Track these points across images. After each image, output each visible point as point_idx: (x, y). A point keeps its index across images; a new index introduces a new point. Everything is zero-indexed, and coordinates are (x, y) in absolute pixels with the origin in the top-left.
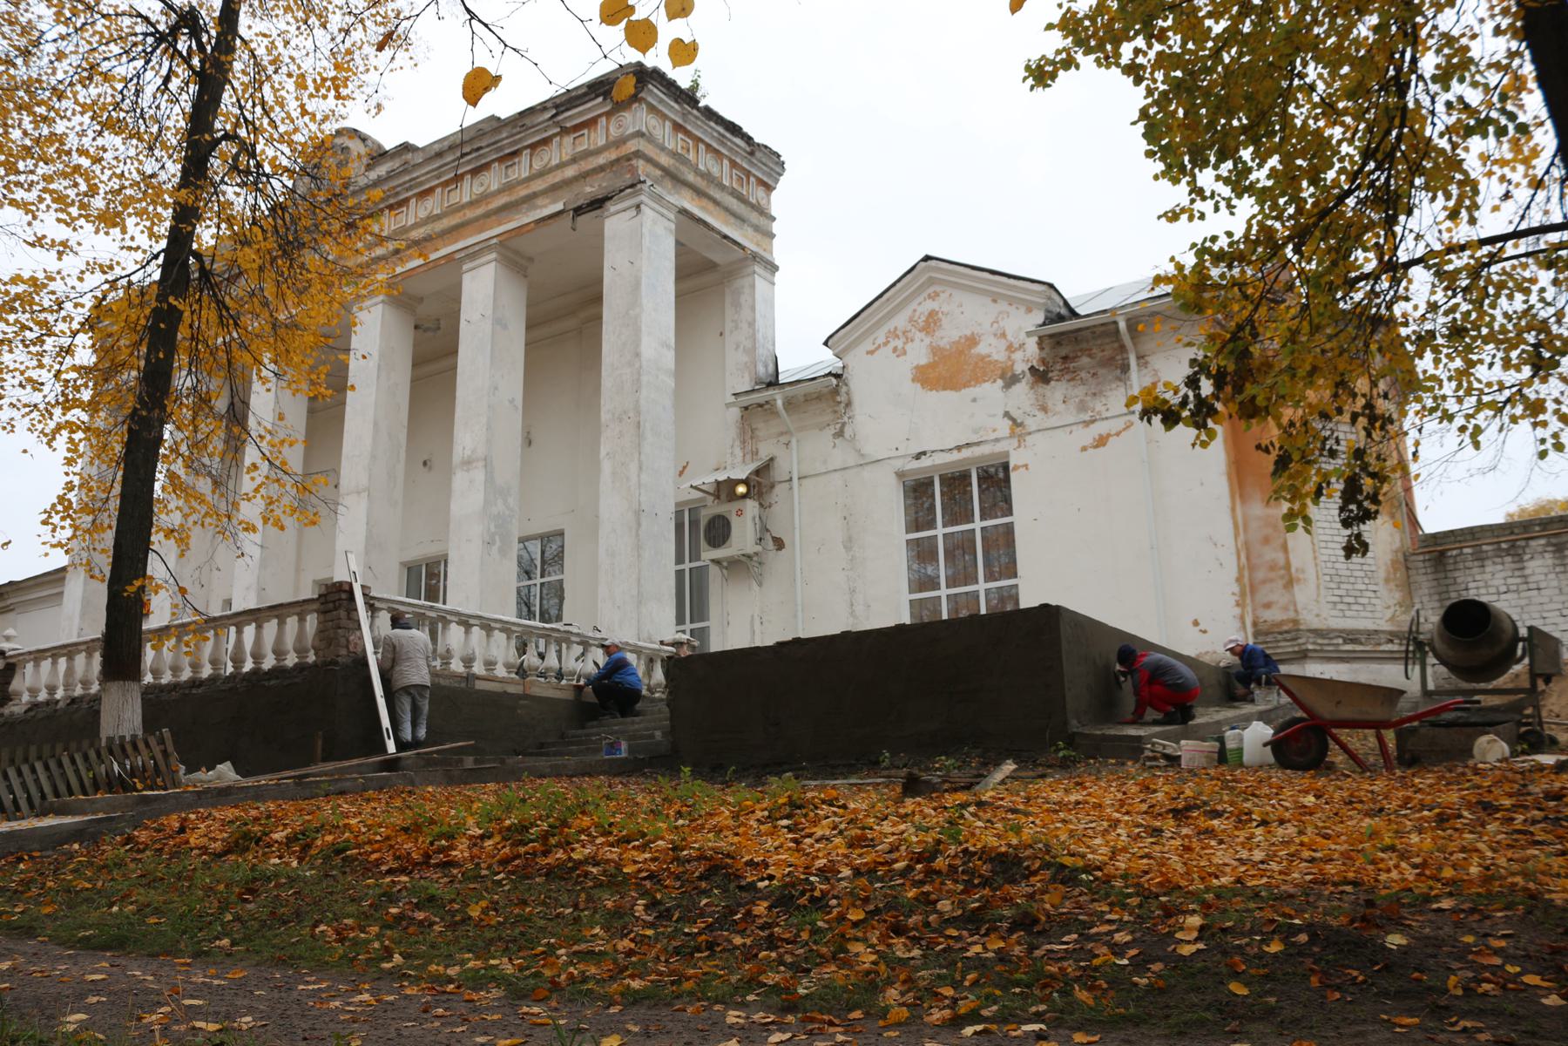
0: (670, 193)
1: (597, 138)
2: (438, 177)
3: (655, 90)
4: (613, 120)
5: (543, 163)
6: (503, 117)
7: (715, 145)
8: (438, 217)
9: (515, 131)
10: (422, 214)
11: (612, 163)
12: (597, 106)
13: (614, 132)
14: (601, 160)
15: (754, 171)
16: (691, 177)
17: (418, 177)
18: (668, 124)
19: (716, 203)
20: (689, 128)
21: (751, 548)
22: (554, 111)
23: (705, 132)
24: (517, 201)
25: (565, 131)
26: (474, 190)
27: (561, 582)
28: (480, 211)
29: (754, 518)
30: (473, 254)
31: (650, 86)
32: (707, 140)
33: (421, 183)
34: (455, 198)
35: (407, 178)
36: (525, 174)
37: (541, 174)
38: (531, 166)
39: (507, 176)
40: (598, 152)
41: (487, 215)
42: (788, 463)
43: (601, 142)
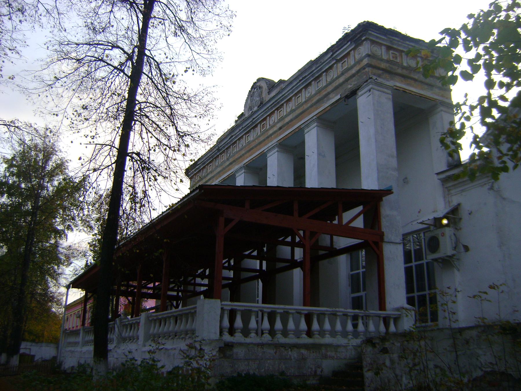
1: (351, 61)
2: (292, 92)
3: (373, 33)
4: (356, 52)
5: (331, 78)
6: (286, 79)
10: (289, 110)
11: (358, 71)
13: (357, 57)
14: (353, 71)
16: (399, 71)
17: (285, 94)
18: (383, 47)
19: (415, 80)
20: (395, 47)
21: (449, 251)
22: (331, 53)
25: (338, 61)
26: (306, 95)
27: (352, 270)
28: (309, 105)
29: (450, 237)
30: (307, 125)
31: (370, 32)
33: (286, 97)
35: (281, 95)
36: (324, 84)
37: (331, 83)
38: (326, 80)
40: (352, 67)
41: (311, 106)
42: (466, 207)
43: (352, 63)
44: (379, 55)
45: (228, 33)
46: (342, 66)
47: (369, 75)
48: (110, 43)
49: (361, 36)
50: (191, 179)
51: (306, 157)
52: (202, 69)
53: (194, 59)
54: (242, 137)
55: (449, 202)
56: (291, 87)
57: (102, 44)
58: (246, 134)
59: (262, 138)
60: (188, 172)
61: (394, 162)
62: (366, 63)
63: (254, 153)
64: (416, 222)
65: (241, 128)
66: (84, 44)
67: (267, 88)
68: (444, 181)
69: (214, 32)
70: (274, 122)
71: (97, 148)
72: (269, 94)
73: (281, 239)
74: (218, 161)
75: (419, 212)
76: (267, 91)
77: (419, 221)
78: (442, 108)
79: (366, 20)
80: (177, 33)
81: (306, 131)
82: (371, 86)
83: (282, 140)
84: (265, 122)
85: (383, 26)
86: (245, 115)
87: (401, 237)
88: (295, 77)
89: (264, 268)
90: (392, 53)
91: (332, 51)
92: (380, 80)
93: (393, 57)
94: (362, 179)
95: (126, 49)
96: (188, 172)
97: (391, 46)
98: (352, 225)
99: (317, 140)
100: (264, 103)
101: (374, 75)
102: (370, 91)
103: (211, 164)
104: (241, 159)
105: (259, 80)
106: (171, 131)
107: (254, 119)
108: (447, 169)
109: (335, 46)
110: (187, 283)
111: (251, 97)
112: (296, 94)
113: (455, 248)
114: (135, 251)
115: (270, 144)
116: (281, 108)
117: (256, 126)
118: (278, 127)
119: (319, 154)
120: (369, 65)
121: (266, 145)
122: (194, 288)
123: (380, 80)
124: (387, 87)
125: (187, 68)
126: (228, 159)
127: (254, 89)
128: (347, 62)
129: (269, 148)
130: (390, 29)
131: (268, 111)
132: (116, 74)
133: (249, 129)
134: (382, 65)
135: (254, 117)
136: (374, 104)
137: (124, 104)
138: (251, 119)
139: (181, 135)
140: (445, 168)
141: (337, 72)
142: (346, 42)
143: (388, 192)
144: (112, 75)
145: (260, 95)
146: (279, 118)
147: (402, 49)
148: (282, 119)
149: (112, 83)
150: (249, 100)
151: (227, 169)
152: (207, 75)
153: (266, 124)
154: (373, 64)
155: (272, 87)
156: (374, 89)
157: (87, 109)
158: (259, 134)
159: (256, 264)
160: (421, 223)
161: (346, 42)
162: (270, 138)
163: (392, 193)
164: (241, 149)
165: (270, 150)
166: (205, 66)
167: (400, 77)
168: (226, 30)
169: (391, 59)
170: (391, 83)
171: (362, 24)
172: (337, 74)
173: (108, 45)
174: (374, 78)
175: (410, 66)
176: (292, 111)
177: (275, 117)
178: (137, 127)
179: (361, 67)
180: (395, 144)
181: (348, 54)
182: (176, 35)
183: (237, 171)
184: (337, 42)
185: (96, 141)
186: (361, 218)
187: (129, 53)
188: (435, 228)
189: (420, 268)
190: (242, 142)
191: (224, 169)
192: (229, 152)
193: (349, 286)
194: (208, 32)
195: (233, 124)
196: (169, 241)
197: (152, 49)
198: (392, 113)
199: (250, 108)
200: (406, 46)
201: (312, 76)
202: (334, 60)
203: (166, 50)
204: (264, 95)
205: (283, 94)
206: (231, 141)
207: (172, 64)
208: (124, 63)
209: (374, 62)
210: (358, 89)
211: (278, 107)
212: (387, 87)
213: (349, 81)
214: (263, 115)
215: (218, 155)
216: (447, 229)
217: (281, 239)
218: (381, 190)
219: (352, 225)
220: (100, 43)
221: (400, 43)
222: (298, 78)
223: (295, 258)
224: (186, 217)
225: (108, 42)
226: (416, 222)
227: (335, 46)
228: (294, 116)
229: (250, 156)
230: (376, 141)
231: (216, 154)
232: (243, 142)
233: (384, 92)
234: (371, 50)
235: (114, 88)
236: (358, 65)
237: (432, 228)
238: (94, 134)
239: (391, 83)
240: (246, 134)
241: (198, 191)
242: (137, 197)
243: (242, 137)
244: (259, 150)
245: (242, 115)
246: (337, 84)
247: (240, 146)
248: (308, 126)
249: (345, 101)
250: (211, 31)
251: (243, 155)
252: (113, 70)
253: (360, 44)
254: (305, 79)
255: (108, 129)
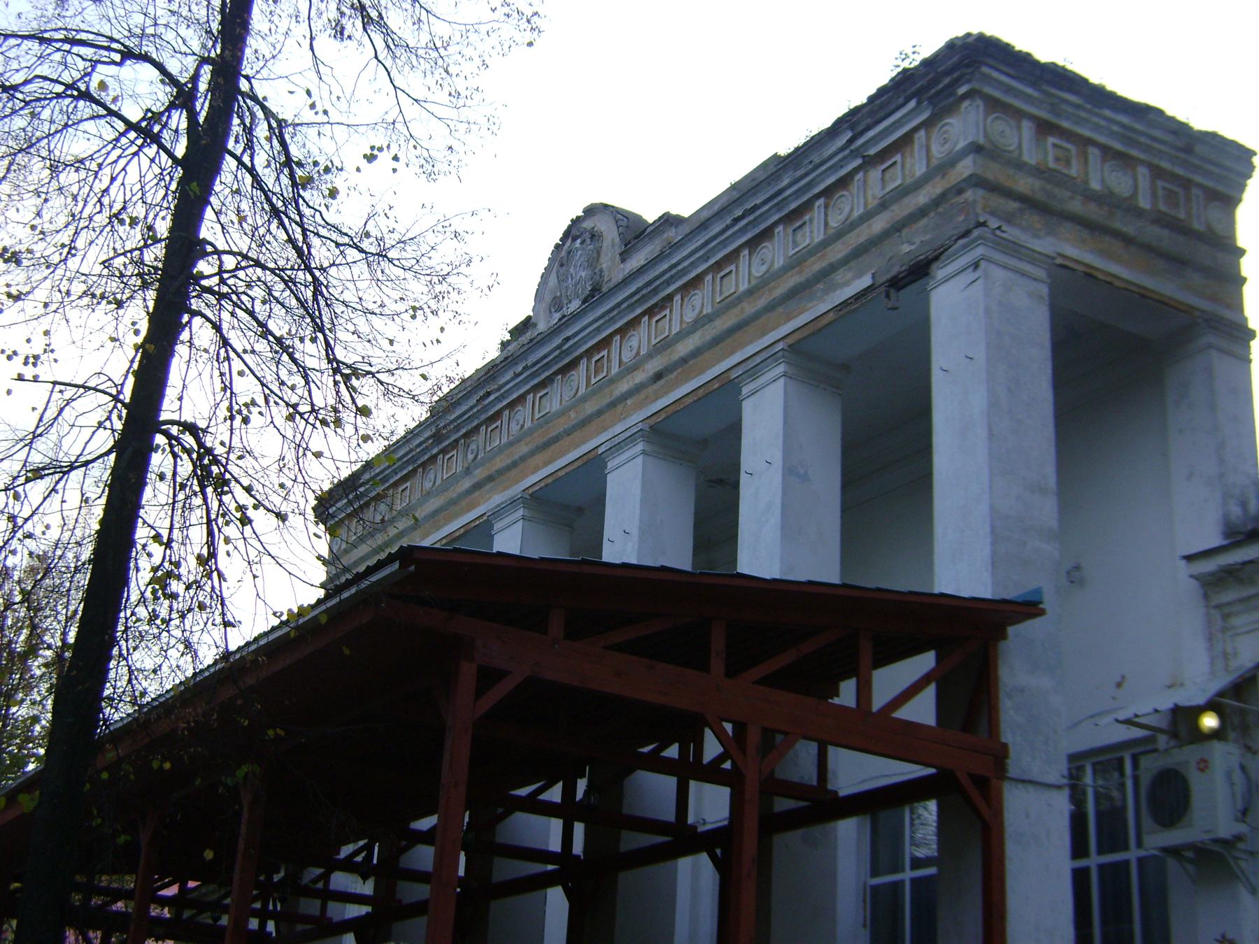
0: (1036, 236)
2: (706, 258)
3: (995, 74)
5: (842, 217)
7: (1118, 146)
8: (710, 319)
9: (799, 173)
10: (690, 317)
12: (909, 115)
13: (938, 151)
15: (1198, 179)
16: (1076, 206)
20: (1066, 124)
21: (1225, 827)
22: (849, 135)
23: (1096, 128)
24: (808, 281)
25: (869, 162)
27: (875, 872)
28: (762, 302)
29: (1229, 775)
30: (753, 369)
31: (985, 69)
32: (1102, 139)
33: (685, 271)
34: (730, 287)
35: (665, 266)
36: (819, 237)
37: (840, 234)
38: (826, 224)
39: (795, 244)
40: (917, 185)
41: (770, 308)
43: (920, 169)
44: (1011, 148)
45: (529, 36)
46: (882, 179)
47: (977, 215)
48: (118, 41)
49: (955, 83)
50: (331, 531)
51: (744, 478)
52: (425, 154)
53: (400, 119)
54: (521, 399)
55: (1225, 655)
56: (702, 241)
57: (83, 43)
58: (535, 389)
59: (590, 408)
60: (325, 508)
61: (1047, 510)
62: (966, 174)
63: (562, 454)
64: (1109, 719)
65: (520, 368)
66: (24, 37)
67: (617, 240)
68: (1212, 584)
69: (483, 29)
70: (638, 353)
71: (56, 395)
72: (623, 261)
73: (646, 749)
74: (432, 475)
75: (1119, 685)
76: (619, 249)
77: (1123, 715)
78: (1211, 338)
79: (975, 31)
80: (343, 29)
81: (745, 391)
82: (980, 251)
83: (663, 416)
84: (605, 353)
85: (1028, 55)
86: (535, 325)
87: (1063, 766)
88: (716, 208)
89: (578, 848)
90: (1055, 145)
91: (852, 128)
92: (1012, 233)
93: (1057, 159)
94: (936, 561)
95: (173, 67)
96: (325, 508)
97: (1054, 120)
98: (903, 713)
99: (785, 423)
100: (605, 289)
101: (993, 213)
102: (976, 266)
103: (408, 484)
104: (514, 472)
105: (591, 211)
106: (312, 355)
107: (568, 339)
108: (1225, 542)
109: (865, 110)
110: (294, 889)
111: (562, 265)
112: (718, 265)
113: (1244, 812)
114: (155, 765)
115: (618, 428)
116: (663, 308)
117: (573, 364)
118: (651, 373)
119: (789, 471)
120: (976, 181)
121: (605, 429)
122: (324, 908)
123: (1012, 233)
124: (1034, 257)
125: (372, 148)
126: (468, 471)
127: (574, 239)
128: (903, 167)
129: (617, 440)
130: (1053, 64)
131: (621, 314)
132: (134, 149)
133: (547, 374)
134: (1022, 182)
135: (569, 333)
136: (987, 311)
137: (155, 254)
138: (558, 341)
139: (346, 374)
140: (1216, 541)
141: (865, 198)
142: (901, 100)
143: (1029, 608)
144: (118, 152)
145: (593, 262)
146: (654, 342)
147: (1086, 133)
148: (665, 345)
149: (113, 179)
150: (554, 275)
151: (464, 503)
152: (440, 178)
153: (609, 360)
154: (989, 176)
155: (636, 238)
156: (989, 261)
157: (18, 263)
158: (582, 391)
159: (550, 833)
160: (1128, 722)
161: (901, 100)
162: (620, 408)
163: (1041, 613)
164: (518, 441)
165: (617, 448)
166: (437, 149)
167: (1078, 227)
168: (522, 28)
169: (1052, 165)
170: (1045, 245)
171: (959, 43)
172: (866, 204)
173: (108, 49)
174: (993, 223)
175: (1112, 193)
176: (701, 321)
177: (641, 339)
178: (200, 332)
179: (947, 186)
180: (1052, 450)
181: (907, 139)
182: (342, 34)
183: (499, 512)
184: (872, 99)
185: (45, 371)
186: (929, 694)
187: (183, 81)
188: (1172, 743)
189: (1115, 876)
190: (519, 417)
191: (453, 502)
192: (473, 446)
193: (865, 926)
194: (463, 28)
195: (494, 353)
196: (282, 733)
197: (258, 76)
198: (1047, 344)
199: (557, 304)
200: (1103, 123)
201: (779, 207)
202: (856, 157)
203: (311, 81)
204: (605, 263)
205: (674, 261)
206: (485, 409)
207: (326, 129)
208: (162, 114)
209: (994, 172)
210: (936, 258)
211: (655, 305)
212: (1034, 257)
213: (905, 232)
214: (598, 330)
215: (434, 457)
216: (1218, 747)
217: (646, 749)
218: (1004, 601)
219: (903, 713)
220: (83, 36)
221: (1083, 114)
222: (730, 212)
223: (690, 820)
224: (347, 652)
225: (112, 39)
226: (1109, 719)
227: (865, 110)
228: (708, 338)
229: (546, 464)
230: (991, 435)
231: (427, 449)
232: (524, 415)
233: (1024, 274)
234: (985, 130)
235: (120, 199)
236: (937, 179)
237: (1162, 741)
238: (39, 351)
239: (1045, 245)
240: (535, 389)
241: (396, 566)
242: (179, 577)
243: (521, 399)
244: (577, 446)
245: (527, 324)
246: (862, 239)
247: (515, 428)
248: (754, 373)
249: (888, 296)
250: (474, 27)
251: (523, 459)
252: (123, 134)
253: (951, 110)
254: (752, 217)
255: (90, 337)
